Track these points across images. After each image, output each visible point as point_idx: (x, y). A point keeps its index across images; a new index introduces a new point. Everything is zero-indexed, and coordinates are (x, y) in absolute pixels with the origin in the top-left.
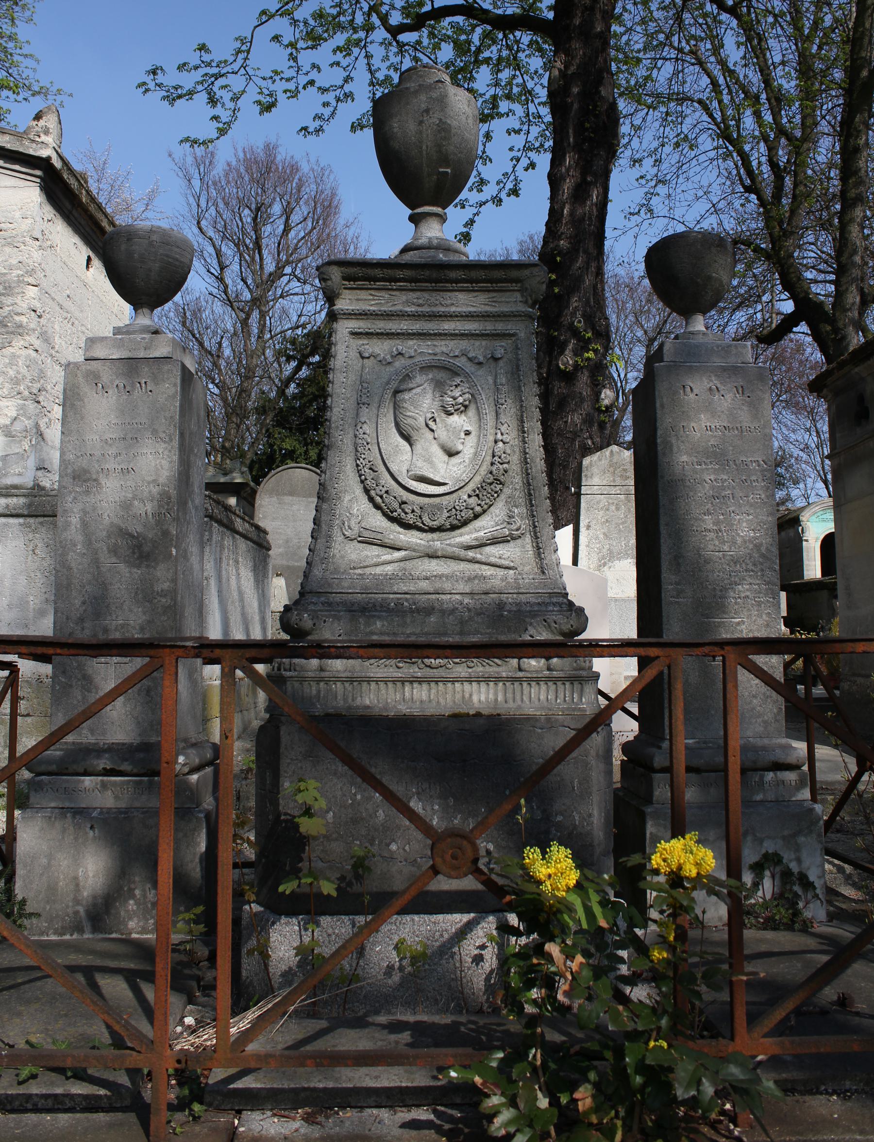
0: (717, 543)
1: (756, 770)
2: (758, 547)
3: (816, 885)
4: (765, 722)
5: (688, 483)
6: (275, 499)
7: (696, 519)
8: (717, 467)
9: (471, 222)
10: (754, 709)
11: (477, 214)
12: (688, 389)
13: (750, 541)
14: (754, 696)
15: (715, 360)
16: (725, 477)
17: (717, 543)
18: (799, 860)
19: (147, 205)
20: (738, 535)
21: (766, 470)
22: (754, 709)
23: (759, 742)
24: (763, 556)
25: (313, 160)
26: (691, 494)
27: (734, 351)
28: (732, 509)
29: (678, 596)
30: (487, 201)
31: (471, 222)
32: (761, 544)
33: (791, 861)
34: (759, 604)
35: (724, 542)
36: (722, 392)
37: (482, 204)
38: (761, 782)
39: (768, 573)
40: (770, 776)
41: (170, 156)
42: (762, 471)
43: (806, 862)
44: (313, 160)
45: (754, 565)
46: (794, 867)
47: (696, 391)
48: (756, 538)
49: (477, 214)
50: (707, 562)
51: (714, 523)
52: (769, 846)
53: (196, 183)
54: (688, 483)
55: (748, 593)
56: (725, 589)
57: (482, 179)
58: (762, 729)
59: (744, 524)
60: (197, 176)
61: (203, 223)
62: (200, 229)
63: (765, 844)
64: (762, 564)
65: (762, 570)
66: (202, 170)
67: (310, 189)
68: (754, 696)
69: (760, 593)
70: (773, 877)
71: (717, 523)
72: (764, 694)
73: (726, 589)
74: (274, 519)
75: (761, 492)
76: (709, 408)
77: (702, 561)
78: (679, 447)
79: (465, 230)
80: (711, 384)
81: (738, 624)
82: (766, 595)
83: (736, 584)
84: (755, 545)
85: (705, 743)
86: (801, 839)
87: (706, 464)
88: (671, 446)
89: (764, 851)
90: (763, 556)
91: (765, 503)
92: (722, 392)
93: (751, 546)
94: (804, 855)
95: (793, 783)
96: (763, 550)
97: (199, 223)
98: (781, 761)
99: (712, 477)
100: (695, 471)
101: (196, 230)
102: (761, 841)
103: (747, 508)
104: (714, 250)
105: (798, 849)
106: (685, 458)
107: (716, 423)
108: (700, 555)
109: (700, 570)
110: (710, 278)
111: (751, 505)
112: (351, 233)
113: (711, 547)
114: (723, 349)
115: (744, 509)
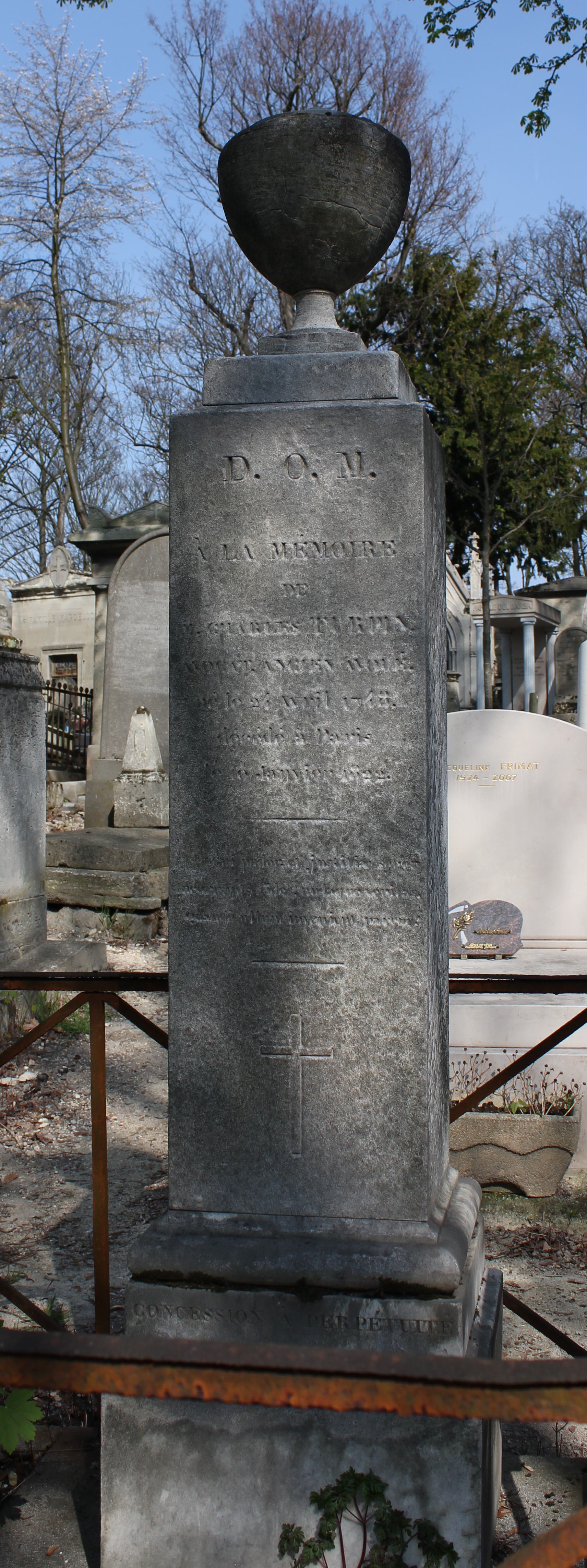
0: (289, 799)
1: (348, 1291)
2: (379, 809)
3: (459, 1549)
4: (382, 1187)
5: (231, 671)
6: (138, 587)
7: (246, 749)
8: (295, 633)
9: (543, 96)
10: (357, 1158)
11: (552, 80)
12: (240, 464)
13: (362, 796)
14: (361, 1132)
15: (316, 394)
16: (312, 655)
17: (289, 799)
18: (422, 1495)
19: (130, 103)
20: (336, 782)
21: (404, 638)
22: (357, 1158)
23: (365, 1230)
24: (390, 828)
25: (379, 10)
26: (237, 693)
27: (357, 373)
28: (323, 725)
29: (201, 913)
30: (569, 57)
31: (543, 96)
32: (387, 803)
33: (404, 1494)
34: (377, 934)
35: (303, 799)
36: (314, 468)
37: (559, 63)
38: (353, 1321)
39: (402, 866)
40: (373, 1308)
41: (152, 22)
42: (397, 639)
43: (440, 1500)
44: (379, 10)
45: (370, 848)
46: (410, 1507)
47: (256, 468)
48: (376, 789)
49: (552, 80)
50: (266, 840)
51: (283, 757)
52: (358, 1459)
53: (195, 62)
54: (231, 671)
55: (353, 910)
56: (301, 901)
57: (565, 18)
58: (375, 1201)
59: (351, 759)
60: (195, 51)
61: (211, 125)
62: (204, 135)
63: (349, 1454)
64: (385, 846)
65: (387, 860)
66: (202, 41)
67: (377, 57)
68: (361, 1132)
69: (380, 909)
70: (363, 1523)
71: (291, 756)
72: (383, 1128)
73: (306, 901)
74: (138, 620)
75: (391, 687)
76: (285, 504)
77: (254, 839)
78: (213, 593)
79: (536, 108)
80: (290, 450)
81: (330, 975)
82: (393, 915)
83: (328, 889)
84: (374, 806)
85: (249, 1223)
86: (429, 1451)
87: (271, 627)
88: (198, 591)
89: (345, 1468)
90: (390, 828)
91: (399, 712)
92: (314, 468)
93: (364, 807)
94: (434, 1484)
95: (425, 1328)
96: (391, 815)
97: (201, 125)
98: (400, 1278)
99: (284, 657)
100: (246, 644)
101: (197, 137)
102: (340, 1447)
103: (358, 722)
104: (324, 151)
105: (420, 1470)
106: (225, 616)
107: (293, 537)
108: (250, 826)
109: (250, 859)
110: (319, 213)
111: (368, 717)
112: (433, 124)
113: (277, 809)
114: (332, 369)
115: (350, 725)
